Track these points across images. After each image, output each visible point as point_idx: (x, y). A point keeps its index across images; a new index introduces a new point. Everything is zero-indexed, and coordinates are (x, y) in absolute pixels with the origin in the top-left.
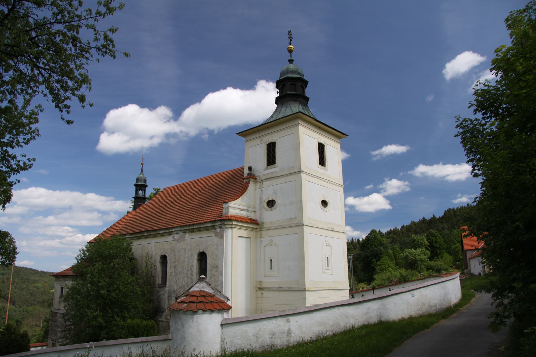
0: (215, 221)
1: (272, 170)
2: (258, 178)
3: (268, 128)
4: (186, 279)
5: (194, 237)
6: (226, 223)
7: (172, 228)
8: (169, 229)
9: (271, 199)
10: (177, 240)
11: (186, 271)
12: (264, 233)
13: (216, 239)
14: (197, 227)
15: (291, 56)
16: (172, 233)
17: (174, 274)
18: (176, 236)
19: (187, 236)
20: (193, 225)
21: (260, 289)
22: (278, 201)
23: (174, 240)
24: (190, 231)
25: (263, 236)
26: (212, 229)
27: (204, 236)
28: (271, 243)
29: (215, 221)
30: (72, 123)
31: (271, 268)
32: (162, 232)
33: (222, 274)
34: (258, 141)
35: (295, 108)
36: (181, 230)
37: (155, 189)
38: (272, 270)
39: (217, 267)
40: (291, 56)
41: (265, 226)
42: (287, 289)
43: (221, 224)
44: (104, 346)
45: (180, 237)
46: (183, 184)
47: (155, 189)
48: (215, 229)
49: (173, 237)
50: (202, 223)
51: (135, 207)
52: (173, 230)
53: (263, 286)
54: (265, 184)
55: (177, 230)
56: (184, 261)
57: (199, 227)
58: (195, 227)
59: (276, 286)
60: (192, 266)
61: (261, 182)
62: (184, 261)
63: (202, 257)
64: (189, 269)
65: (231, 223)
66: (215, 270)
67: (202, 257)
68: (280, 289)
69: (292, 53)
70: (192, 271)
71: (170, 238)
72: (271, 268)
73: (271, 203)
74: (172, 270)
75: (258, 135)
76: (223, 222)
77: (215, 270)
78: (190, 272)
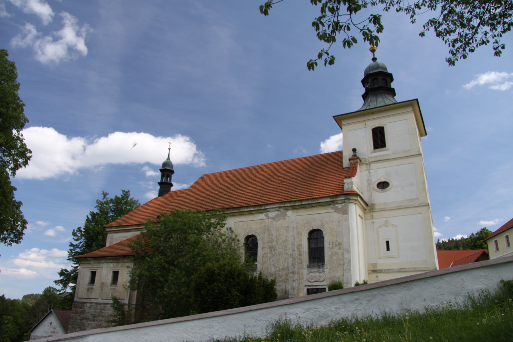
0: (337, 195)
1: (380, 153)
2: (363, 161)
3: (373, 113)
4: (291, 260)
5: (301, 214)
6: (351, 198)
7: (267, 205)
8: (261, 206)
9: (383, 180)
10: (274, 218)
11: (290, 252)
12: (375, 214)
13: (336, 216)
14: (307, 203)
15: (374, 55)
16: (264, 211)
17: (270, 255)
18: (271, 214)
19: (290, 213)
20: (301, 201)
21: (374, 271)
22: (393, 183)
23: (268, 218)
24: (293, 208)
25: (374, 217)
26: (329, 205)
27: (317, 212)
28: (386, 224)
29: (337, 196)
30: (420, 35)
31: (388, 249)
32: (249, 210)
33: (349, 252)
34: (362, 125)
35: (382, 101)
36: (280, 207)
37: (123, 191)
38: (389, 252)
39: (340, 244)
40: (374, 55)
41: (377, 207)
42: (411, 270)
43: (345, 199)
44: (363, 291)
45: (277, 215)
46: (239, 170)
47: (123, 191)
48: (334, 204)
49: (267, 216)
50: (316, 198)
51: (159, 196)
52: (267, 207)
53: (379, 268)
54: (373, 166)
55: (274, 206)
56: (286, 241)
57: (310, 202)
58: (303, 203)
59: (396, 267)
60: (300, 245)
61: (369, 164)
62: (286, 241)
63: (316, 237)
64: (296, 248)
65: (355, 198)
66: (338, 247)
67: (316, 237)
68: (402, 270)
69: (375, 53)
70: (300, 251)
71: (262, 216)
72: (388, 249)
73: (383, 185)
74: (267, 250)
75: (362, 119)
76: (348, 197)
77: (338, 247)
78: (296, 252)
